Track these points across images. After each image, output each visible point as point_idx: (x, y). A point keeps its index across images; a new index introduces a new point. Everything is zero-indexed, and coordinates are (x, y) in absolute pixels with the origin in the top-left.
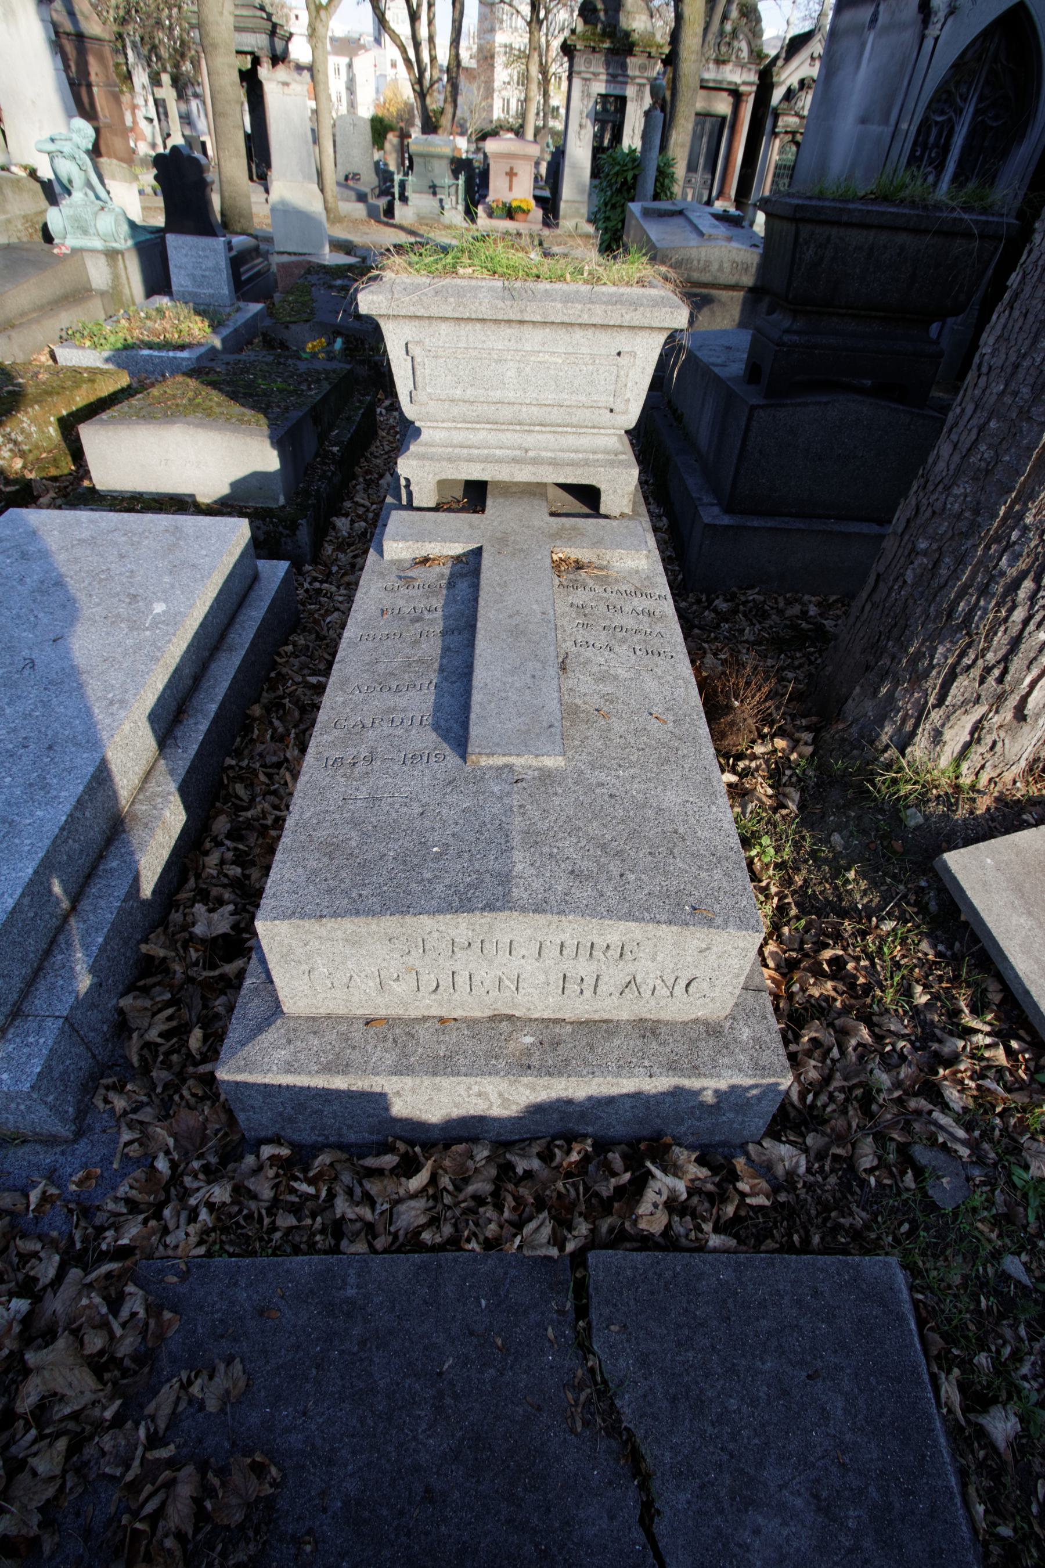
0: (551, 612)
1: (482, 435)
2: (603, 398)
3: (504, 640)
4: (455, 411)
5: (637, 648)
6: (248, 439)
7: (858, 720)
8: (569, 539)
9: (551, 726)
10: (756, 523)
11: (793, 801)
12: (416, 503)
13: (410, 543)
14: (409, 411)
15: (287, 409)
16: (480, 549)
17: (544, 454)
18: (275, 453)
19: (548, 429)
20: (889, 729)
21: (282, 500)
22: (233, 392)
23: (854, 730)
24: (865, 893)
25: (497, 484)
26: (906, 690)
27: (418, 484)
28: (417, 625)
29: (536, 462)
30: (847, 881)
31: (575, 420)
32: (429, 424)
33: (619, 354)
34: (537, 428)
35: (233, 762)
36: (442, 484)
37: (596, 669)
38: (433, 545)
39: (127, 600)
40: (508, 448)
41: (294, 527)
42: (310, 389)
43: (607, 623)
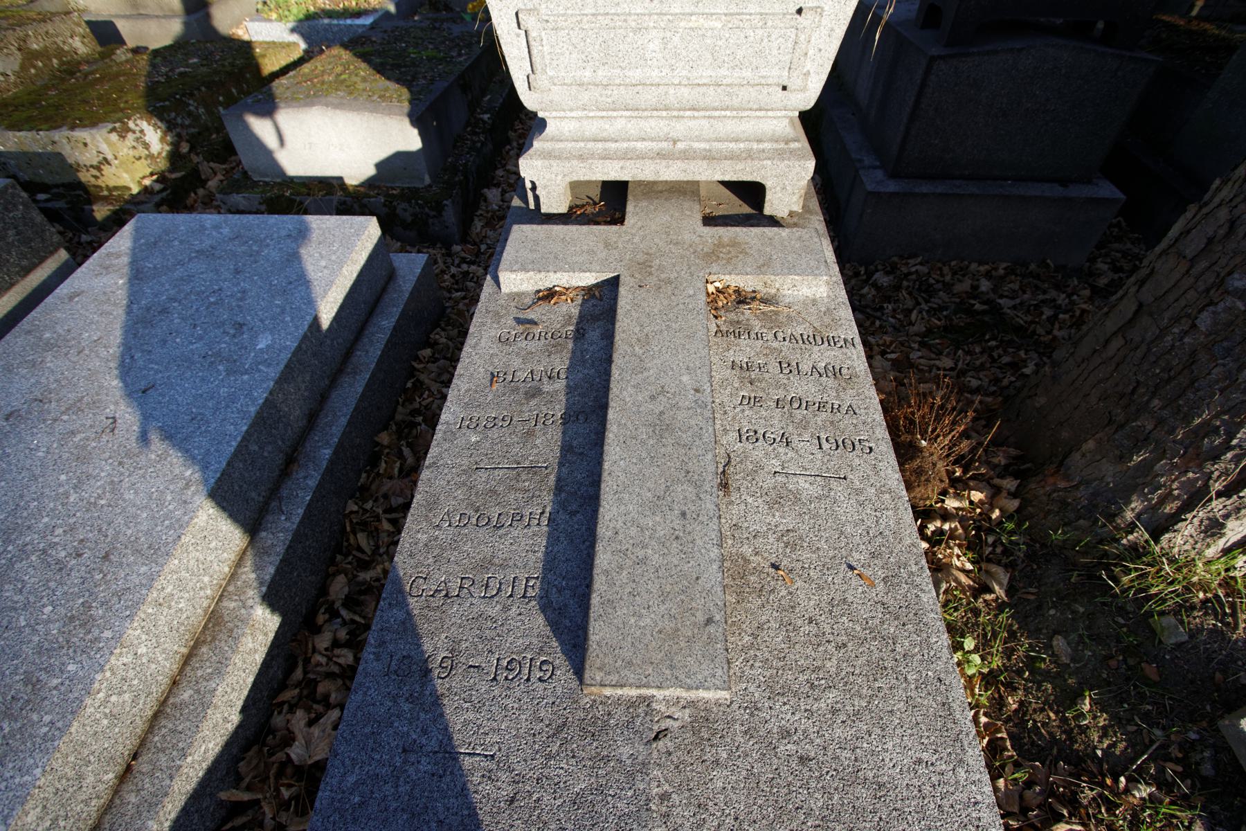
0: (707, 387)
1: (620, 124)
2: (775, 72)
3: (643, 443)
4: (585, 97)
5: (823, 436)
6: (387, 119)
7: (1088, 483)
8: (729, 261)
9: (709, 621)
10: (925, 188)
11: (1000, 584)
12: (544, 209)
13: (533, 270)
14: (529, 100)
15: (432, 80)
16: (616, 279)
17: (696, 145)
18: (416, 131)
19: (702, 113)
20: (1136, 505)
21: (427, 180)
22: (382, 64)
23: (1083, 492)
24: (1105, 735)
25: (640, 183)
26: (1174, 466)
27: (545, 187)
28: (533, 402)
29: (686, 156)
30: (1082, 715)
31: (736, 102)
32: (554, 114)
33: (800, 11)
34: (688, 113)
35: (355, 508)
36: (575, 186)
37: (770, 482)
38: (558, 275)
39: (232, 331)
40: (652, 140)
41: (439, 208)
42: (460, 55)
43: (781, 394)
